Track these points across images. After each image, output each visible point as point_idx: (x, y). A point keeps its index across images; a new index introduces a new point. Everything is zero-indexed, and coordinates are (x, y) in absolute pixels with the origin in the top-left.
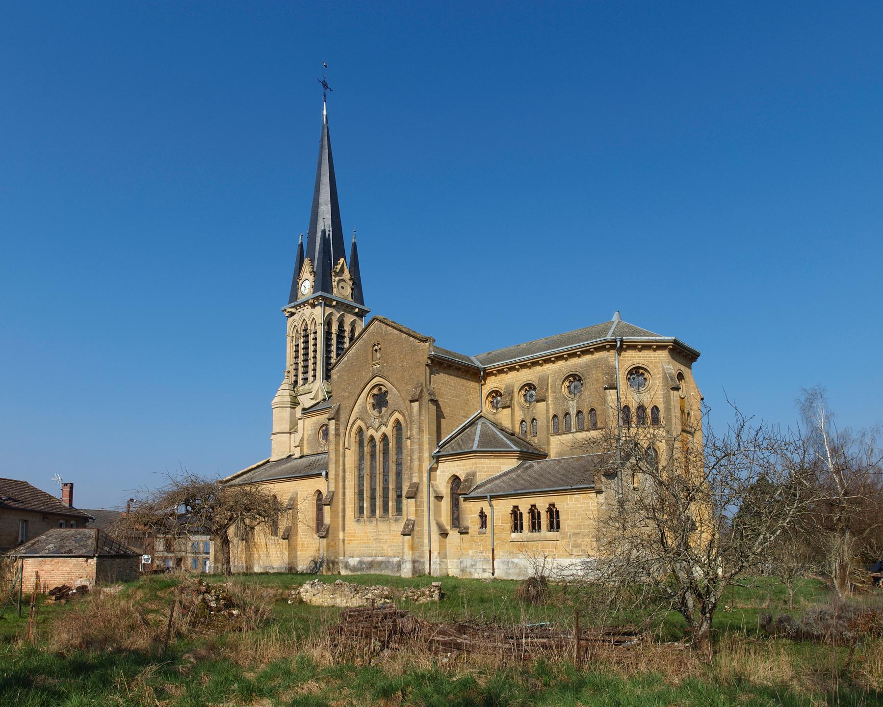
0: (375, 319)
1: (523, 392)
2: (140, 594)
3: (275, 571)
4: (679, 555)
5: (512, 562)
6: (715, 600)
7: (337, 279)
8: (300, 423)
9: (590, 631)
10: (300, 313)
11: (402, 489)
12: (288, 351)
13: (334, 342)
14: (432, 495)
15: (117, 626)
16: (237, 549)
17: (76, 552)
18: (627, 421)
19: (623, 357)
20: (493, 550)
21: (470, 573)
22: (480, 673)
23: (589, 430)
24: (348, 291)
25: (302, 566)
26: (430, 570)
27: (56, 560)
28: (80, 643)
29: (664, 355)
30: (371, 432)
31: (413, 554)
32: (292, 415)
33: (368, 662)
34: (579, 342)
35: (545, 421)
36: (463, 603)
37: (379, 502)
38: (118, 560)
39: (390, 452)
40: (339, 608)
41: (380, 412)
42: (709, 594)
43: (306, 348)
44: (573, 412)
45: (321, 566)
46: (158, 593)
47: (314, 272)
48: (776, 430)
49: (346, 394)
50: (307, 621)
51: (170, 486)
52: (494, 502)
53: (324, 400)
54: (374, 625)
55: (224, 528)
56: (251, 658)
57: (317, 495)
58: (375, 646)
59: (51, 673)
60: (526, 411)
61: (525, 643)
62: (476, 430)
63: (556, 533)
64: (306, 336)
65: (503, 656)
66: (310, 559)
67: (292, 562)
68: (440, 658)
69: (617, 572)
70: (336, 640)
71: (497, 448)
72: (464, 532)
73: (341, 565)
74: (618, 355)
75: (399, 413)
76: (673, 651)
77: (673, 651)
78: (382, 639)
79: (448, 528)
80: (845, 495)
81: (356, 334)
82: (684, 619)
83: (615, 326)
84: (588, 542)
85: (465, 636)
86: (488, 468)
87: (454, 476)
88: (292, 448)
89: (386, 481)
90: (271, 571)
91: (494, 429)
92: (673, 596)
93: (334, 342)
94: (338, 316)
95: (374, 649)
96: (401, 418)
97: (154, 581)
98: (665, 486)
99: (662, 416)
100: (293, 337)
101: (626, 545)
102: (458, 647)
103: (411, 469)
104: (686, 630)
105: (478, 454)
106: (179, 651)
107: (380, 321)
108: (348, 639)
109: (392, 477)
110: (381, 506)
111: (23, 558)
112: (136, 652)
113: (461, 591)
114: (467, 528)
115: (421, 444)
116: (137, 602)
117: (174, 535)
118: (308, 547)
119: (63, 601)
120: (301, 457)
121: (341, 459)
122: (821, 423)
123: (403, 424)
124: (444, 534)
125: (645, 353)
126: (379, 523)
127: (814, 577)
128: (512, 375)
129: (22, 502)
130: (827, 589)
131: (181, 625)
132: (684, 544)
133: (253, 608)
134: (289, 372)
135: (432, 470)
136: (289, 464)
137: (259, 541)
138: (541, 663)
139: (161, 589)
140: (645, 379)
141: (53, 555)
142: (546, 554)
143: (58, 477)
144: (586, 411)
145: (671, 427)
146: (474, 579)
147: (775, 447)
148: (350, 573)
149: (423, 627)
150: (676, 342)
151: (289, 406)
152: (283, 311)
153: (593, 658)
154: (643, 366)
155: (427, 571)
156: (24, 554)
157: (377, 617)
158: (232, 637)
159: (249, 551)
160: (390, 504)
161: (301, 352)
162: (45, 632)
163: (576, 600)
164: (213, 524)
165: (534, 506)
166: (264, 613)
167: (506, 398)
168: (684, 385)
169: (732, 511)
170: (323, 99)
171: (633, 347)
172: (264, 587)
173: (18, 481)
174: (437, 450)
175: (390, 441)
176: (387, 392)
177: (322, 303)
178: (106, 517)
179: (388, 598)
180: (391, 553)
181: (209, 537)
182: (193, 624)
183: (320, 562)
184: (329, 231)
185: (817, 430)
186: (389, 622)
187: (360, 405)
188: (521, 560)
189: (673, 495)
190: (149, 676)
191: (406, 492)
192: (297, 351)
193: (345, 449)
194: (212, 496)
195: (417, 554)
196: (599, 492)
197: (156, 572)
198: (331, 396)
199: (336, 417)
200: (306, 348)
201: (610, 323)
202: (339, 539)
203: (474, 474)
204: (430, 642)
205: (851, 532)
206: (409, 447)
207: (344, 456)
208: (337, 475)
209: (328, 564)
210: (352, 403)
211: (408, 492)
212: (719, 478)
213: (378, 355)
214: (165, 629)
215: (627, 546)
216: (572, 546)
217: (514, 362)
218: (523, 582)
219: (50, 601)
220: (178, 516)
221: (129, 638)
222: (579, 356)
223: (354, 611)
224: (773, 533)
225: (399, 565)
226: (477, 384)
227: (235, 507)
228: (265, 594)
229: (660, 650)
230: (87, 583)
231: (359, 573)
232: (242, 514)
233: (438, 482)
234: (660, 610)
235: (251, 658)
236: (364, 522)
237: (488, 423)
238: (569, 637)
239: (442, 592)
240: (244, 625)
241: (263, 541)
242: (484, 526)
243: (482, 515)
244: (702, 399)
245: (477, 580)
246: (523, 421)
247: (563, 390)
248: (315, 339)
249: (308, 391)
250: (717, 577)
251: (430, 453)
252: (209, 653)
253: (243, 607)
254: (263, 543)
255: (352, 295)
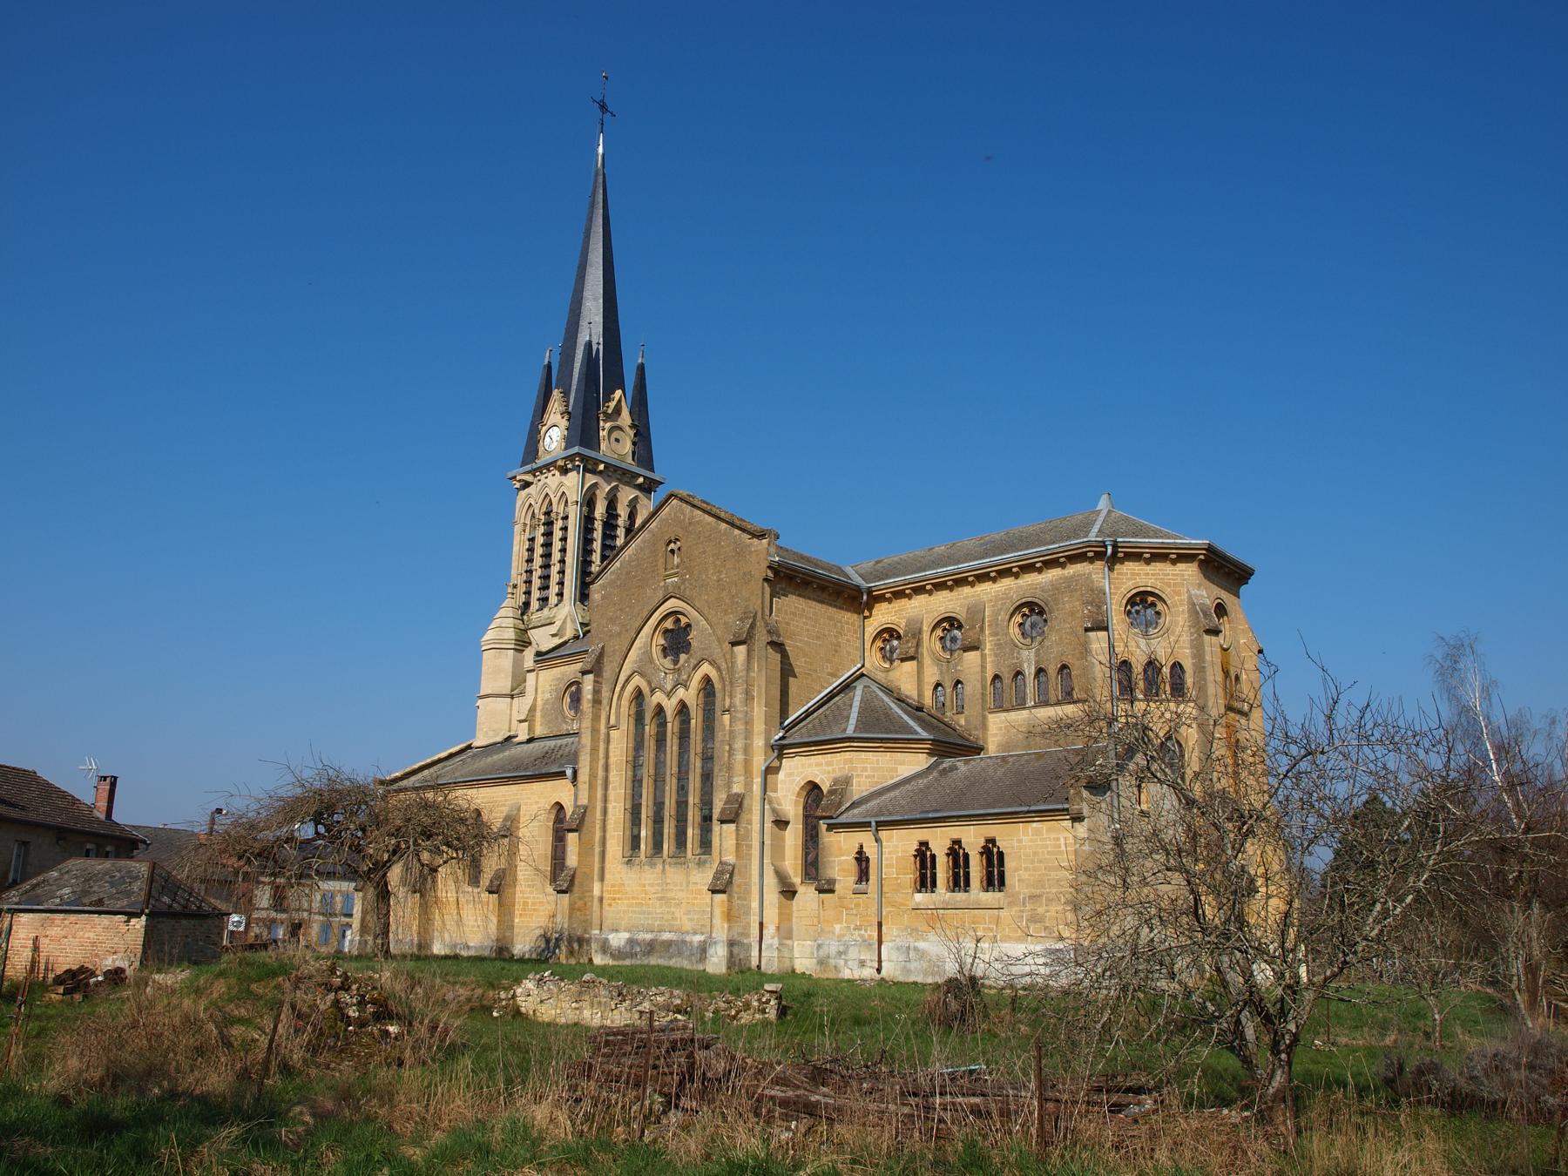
0: (672, 495)
1: (939, 632)
2: (220, 988)
3: (472, 953)
4: (1228, 939)
5: (916, 949)
6: (1297, 1027)
7: (608, 425)
8: (531, 677)
9: (1064, 1084)
10: (540, 483)
11: (711, 804)
12: (516, 548)
13: (598, 534)
14: (769, 818)
15: (173, 1048)
16: (404, 909)
17: (110, 904)
18: (1127, 689)
19: (1118, 574)
20: (880, 925)
21: (835, 967)
22: (854, 1161)
23: (1058, 703)
24: (627, 447)
25: (522, 945)
26: (760, 961)
27: (73, 917)
28: (102, 1079)
29: (1190, 571)
30: (659, 697)
31: (730, 928)
32: (517, 664)
33: (638, 1134)
34: (1040, 546)
35: (979, 686)
36: (821, 1026)
37: (669, 829)
38: (184, 922)
39: (692, 736)
40: (588, 1028)
41: (676, 662)
42: (1286, 1016)
43: (548, 545)
44: (1029, 671)
45: (557, 946)
46: (254, 987)
47: (569, 413)
48: (1395, 709)
49: (616, 628)
50: (527, 1052)
51: (290, 787)
52: (883, 834)
53: (576, 637)
54: (651, 1062)
55: (382, 867)
56: (418, 1119)
57: (554, 812)
58: (652, 1103)
59: (40, 1135)
60: (944, 667)
61: (940, 1105)
62: (852, 699)
63: (998, 895)
64: (549, 524)
65: (897, 1128)
66: (539, 932)
67: (504, 937)
68: (776, 1131)
69: (1112, 969)
70: (579, 1088)
71: (891, 732)
72: (827, 889)
73: (594, 946)
74: (1109, 569)
75: (710, 663)
76: (1221, 1125)
77: (1221, 1125)
78: (666, 1089)
79: (797, 880)
80: (1528, 830)
81: (638, 522)
82: (1239, 1064)
83: (1102, 519)
84: (1056, 911)
85: (825, 1089)
86: (873, 769)
87: (810, 782)
88: (515, 723)
89: (682, 789)
90: (464, 953)
91: (886, 699)
92: (1218, 1018)
93: (598, 534)
94: (607, 490)
95: (651, 1109)
96: (713, 674)
97: (248, 964)
98: (1199, 809)
99: (1189, 680)
100: (525, 524)
101: (1129, 919)
102: (811, 1110)
103: (730, 767)
104: (1243, 1084)
105: (855, 744)
106: (283, 1101)
107: (681, 499)
108: (601, 1087)
109: (694, 783)
110: (672, 836)
111: (13, 912)
112: (203, 1099)
113: (820, 1002)
114: (832, 882)
115: (748, 723)
116: (214, 1003)
117: (289, 879)
118: (535, 910)
119: (78, 997)
120: (530, 741)
121: (602, 746)
122: (1475, 699)
123: (718, 686)
124: (789, 892)
125: (1157, 567)
126: (667, 867)
127: (1480, 988)
128: (919, 601)
129: (23, 808)
130: (1504, 1011)
131: (291, 1051)
132: (1236, 919)
133: (426, 1021)
134: (515, 586)
135: (770, 771)
136: (507, 753)
137: (444, 895)
138: (970, 1145)
139: (260, 980)
140: (1158, 613)
141: (68, 908)
142: (978, 934)
143: (91, 764)
144: (1052, 670)
145: (1206, 701)
146: (843, 980)
147: (1397, 739)
148: (611, 962)
149: (744, 1069)
150: (1210, 549)
151: (513, 646)
152: (510, 479)
153: (1069, 1136)
154: (1152, 590)
155: (754, 963)
156: (16, 904)
157: (658, 1048)
158: (385, 1075)
159: (426, 913)
160: (690, 832)
161: (539, 551)
162: (38, 1055)
163: (1033, 1024)
164: (363, 860)
165: (957, 842)
166: (446, 1031)
167: (908, 641)
168: (1227, 626)
169: (1321, 858)
170: (599, 126)
171: (1136, 557)
172: (448, 982)
173: (18, 770)
174: (781, 734)
175: (693, 714)
176: (689, 625)
177: (579, 466)
178: (169, 840)
179: (679, 1012)
180: (688, 926)
181: (354, 884)
182: (314, 1049)
183: (556, 939)
184: (598, 344)
185: (1468, 711)
186: (681, 1056)
187: (640, 649)
188: (932, 945)
189: (1214, 824)
190: (224, 1146)
191: (719, 810)
192: (531, 550)
193: (609, 728)
194: (363, 807)
195: (737, 929)
196: (1078, 819)
197: (251, 947)
198: (589, 631)
199: (596, 669)
200: (548, 545)
201: (1093, 512)
202: (592, 897)
203: (847, 781)
204: (758, 1100)
205: (1543, 902)
206: (728, 728)
207: (608, 742)
208: (593, 776)
209: (570, 943)
210: (626, 645)
211: (723, 810)
212: (1296, 795)
213: (676, 560)
214: (262, 1056)
215: (1131, 921)
216: (1028, 920)
217: (922, 579)
218: (937, 986)
219: (53, 996)
220: (301, 843)
221: (192, 1071)
222: (1040, 571)
223: (615, 1034)
224: (1400, 900)
225: (703, 950)
226: (855, 616)
227: (404, 830)
228: (450, 996)
229: (1195, 1124)
230: (124, 964)
231: (628, 962)
232: (416, 843)
233: (780, 794)
234: (1192, 1045)
235: (418, 1119)
236: (641, 864)
237: (874, 687)
238: (1023, 1094)
239: (784, 1003)
240: (408, 1053)
241: (452, 896)
242: (864, 878)
243: (861, 859)
244: (1260, 651)
245: (849, 981)
246: (938, 685)
247: (1011, 631)
248: (565, 529)
249: (548, 621)
250: (1298, 983)
251: (767, 740)
252: (340, 1104)
253: (408, 1021)
254: (452, 899)
255: (634, 453)
